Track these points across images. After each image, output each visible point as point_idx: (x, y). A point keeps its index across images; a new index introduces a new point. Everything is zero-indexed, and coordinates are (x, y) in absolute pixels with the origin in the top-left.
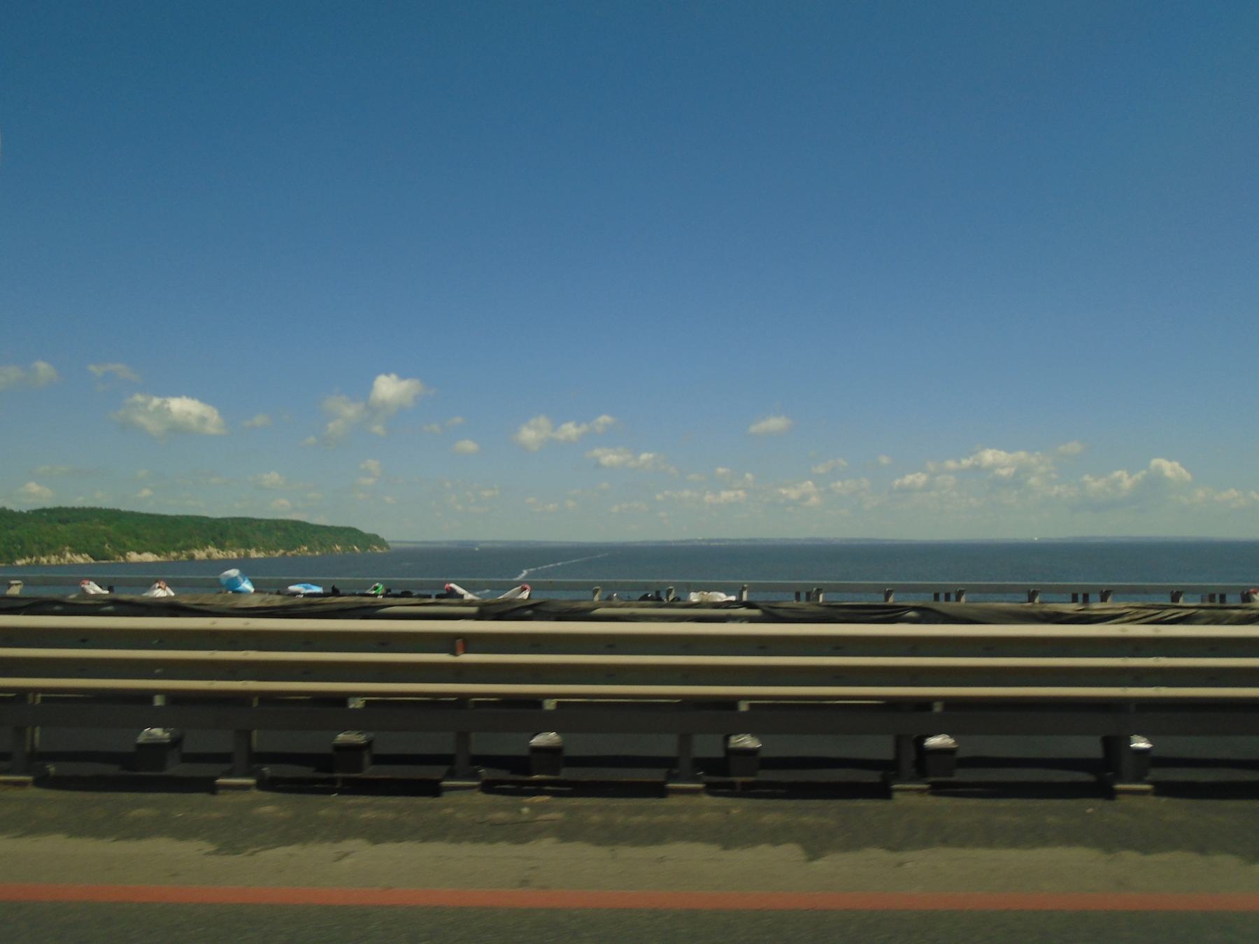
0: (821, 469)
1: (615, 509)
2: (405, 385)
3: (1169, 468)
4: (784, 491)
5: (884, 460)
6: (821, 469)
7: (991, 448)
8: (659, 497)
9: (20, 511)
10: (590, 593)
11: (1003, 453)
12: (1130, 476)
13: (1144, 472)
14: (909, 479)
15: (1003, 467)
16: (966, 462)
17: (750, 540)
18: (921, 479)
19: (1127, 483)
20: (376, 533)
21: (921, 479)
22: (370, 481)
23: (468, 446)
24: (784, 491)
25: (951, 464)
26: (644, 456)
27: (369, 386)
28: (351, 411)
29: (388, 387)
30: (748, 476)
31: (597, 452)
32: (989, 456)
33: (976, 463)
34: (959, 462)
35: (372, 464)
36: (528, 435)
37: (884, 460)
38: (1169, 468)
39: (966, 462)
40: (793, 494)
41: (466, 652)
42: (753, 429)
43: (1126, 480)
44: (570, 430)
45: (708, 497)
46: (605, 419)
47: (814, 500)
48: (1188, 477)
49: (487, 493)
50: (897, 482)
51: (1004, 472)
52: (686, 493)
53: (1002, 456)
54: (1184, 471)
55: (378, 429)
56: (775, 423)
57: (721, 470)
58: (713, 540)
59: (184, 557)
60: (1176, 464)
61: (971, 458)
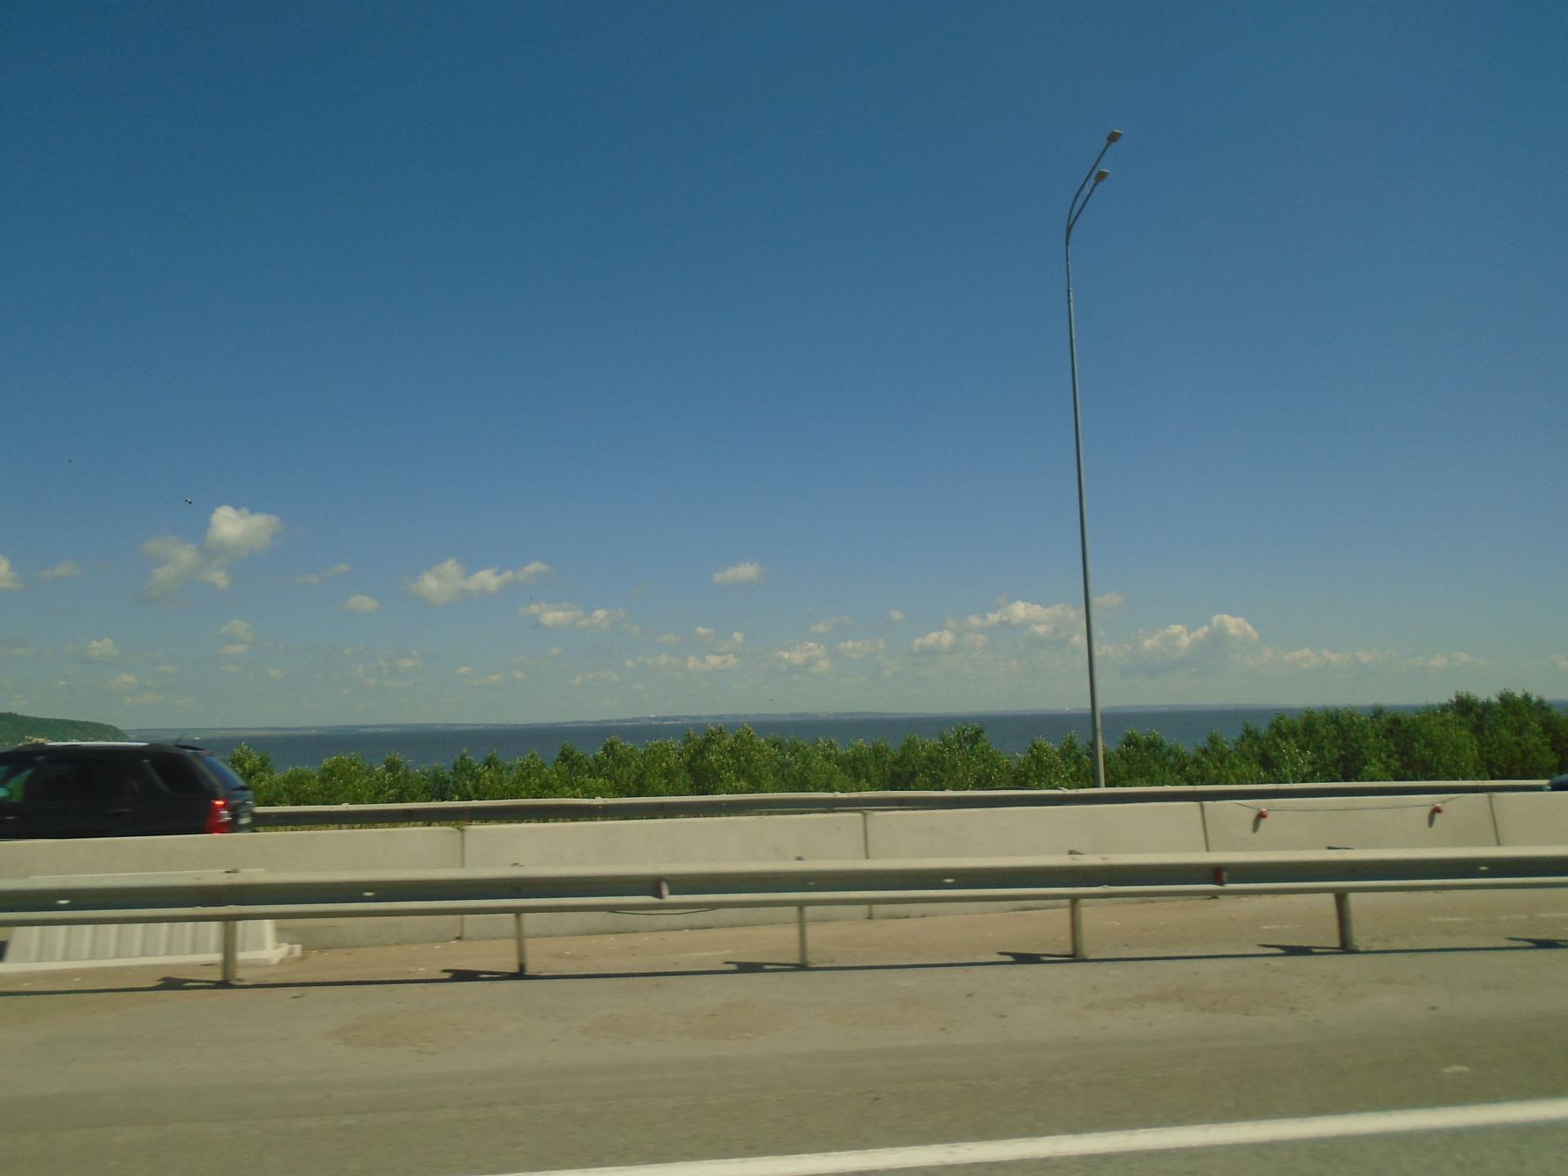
0: (821, 628)
1: (578, 680)
2: (258, 520)
3: (1233, 624)
4: (786, 655)
5: (897, 615)
6: (821, 628)
7: (1023, 601)
8: (629, 663)
9: (1376, 704)
11: (1037, 607)
12: (1189, 635)
13: (1206, 629)
14: (932, 638)
15: (1038, 624)
16: (994, 618)
17: (860, 713)
18: (947, 638)
19: (1185, 641)
21: (947, 638)
22: (240, 649)
23: (364, 602)
24: (786, 655)
25: (975, 620)
26: (600, 614)
27: (206, 524)
28: (185, 555)
29: (229, 524)
30: (738, 636)
31: (534, 609)
32: (1020, 610)
33: (1005, 619)
34: (984, 617)
35: (239, 626)
36: (430, 584)
37: (897, 615)
38: (1233, 624)
39: (994, 618)
40: (797, 657)
41: (1294, 782)
42: (718, 577)
43: (1183, 636)
44: (487, 579)
45: (692, 662)
46: (535, 567)
47: (823, 665)
48: (1255, 635)
49: (407, 663)
50: (917, 642)
51: (1041, 630)
52: (664, 659)
53: (1036, 610)
54: (1249, 627)
55: (219, 578)
56: (747, 571)
57: (701, 630)
58: (665, 719)
59: (1154, 730)
60: (1241, 620)
61: (999, 614)
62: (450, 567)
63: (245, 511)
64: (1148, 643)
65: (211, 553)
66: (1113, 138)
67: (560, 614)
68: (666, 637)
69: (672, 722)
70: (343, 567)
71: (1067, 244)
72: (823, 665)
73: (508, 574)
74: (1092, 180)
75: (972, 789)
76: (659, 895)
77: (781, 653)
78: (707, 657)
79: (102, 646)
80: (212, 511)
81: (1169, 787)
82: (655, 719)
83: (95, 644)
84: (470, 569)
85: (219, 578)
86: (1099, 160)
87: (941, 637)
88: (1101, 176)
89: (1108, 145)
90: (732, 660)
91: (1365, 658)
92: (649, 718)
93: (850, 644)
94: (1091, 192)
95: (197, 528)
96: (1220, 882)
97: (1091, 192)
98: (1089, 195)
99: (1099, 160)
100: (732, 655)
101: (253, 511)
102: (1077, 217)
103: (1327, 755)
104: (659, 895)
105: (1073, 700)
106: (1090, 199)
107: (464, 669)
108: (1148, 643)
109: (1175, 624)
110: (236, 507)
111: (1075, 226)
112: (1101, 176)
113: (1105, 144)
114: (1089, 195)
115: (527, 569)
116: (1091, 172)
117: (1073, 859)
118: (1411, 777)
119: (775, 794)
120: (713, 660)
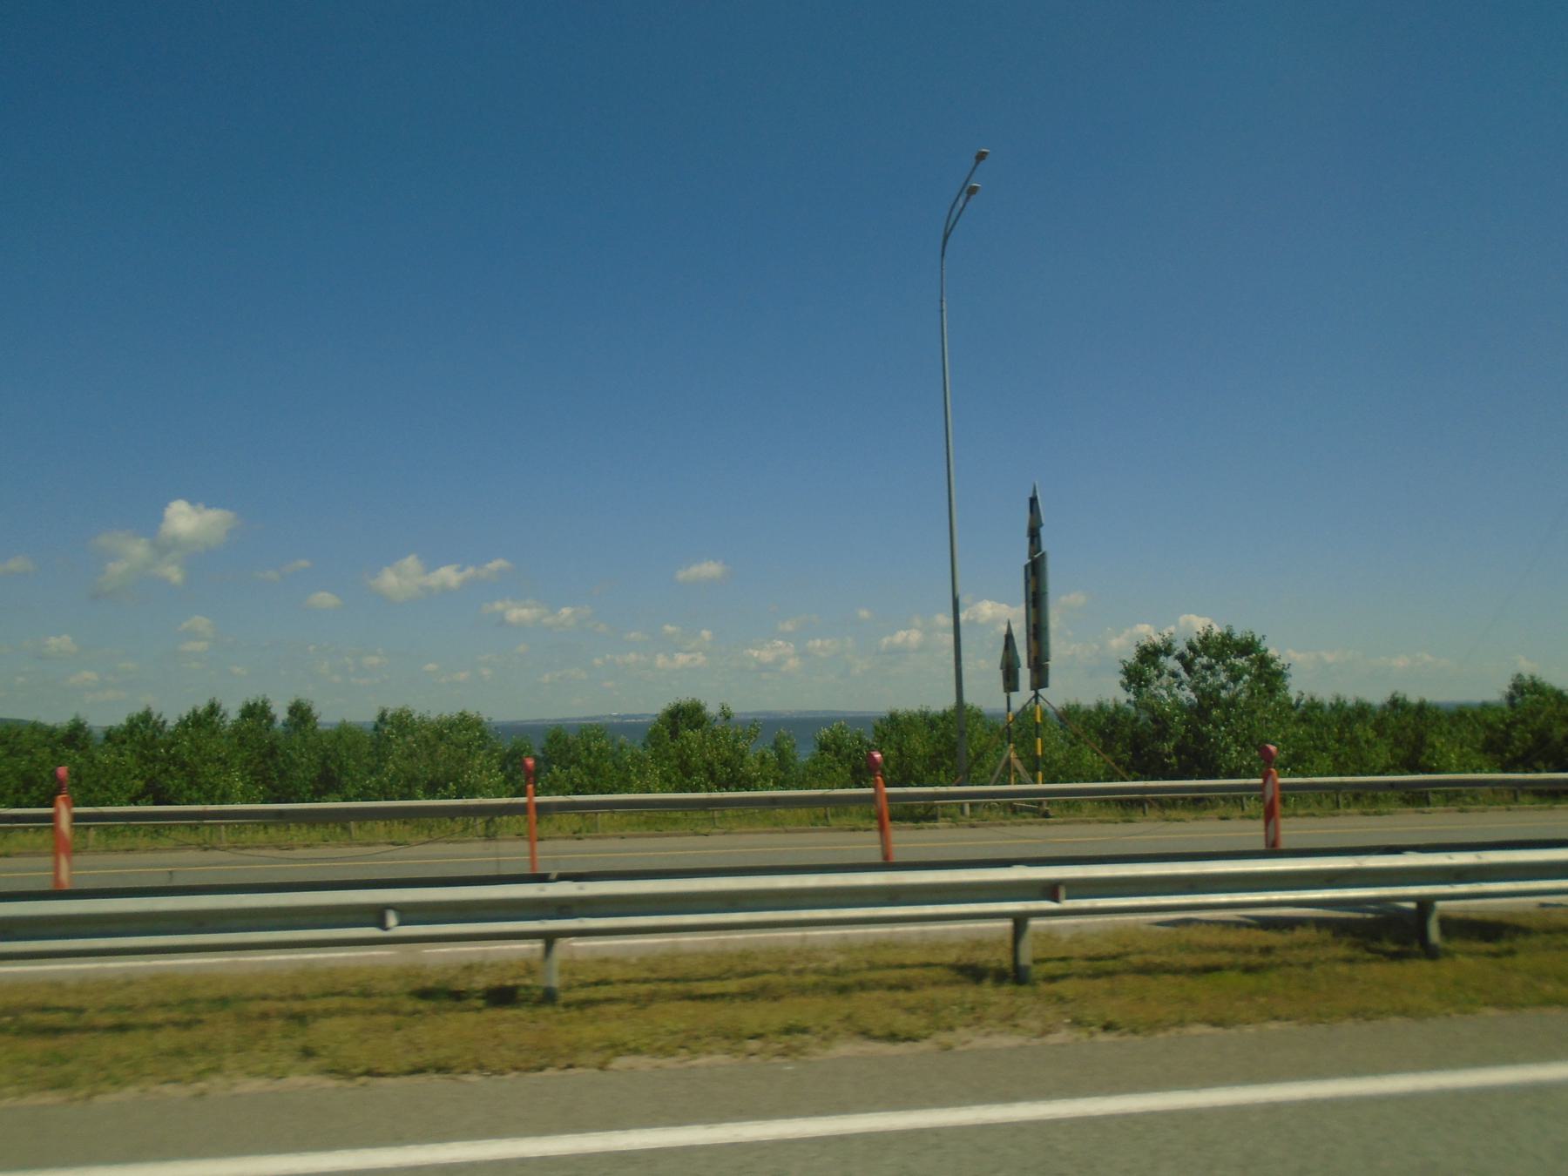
0: (788, 627)
2: (214, 516)
4: (756, 654)
5: (864, 614)
7: (989, 600)
8: (597, 661)
10: (1399, 716)
11: (1004, 606)
14: (900, 636)
17: (824, 712)
18: (915, 636)
20: (393, 706)
21: (915, 636)
22: (201, 646)
23: (325, 599)
24: (756, 654)
26: (566, 611)
27: (160, 518)
28: (139, 549)
29: (183, 519)
31: (499, 606)
33: (971, 618)
35: (200, 622)
36: (389, 580)
37: (864, 614)
40: (767, 656)
42: (681, 575)
44: (449, 575)
45: (661, 660)
47: (793, 663)
50: (885, 640)
52: (632, 657)
55: (174, 574)
56: (710, 569)
57: (669, 628)
62: (411, 562)
63: (201, 506)
64: (1115, 642)
65: (165, 548)
66: (981, 156)
67: (525, 612)
68: (633, 635)
69: (633, 720)
70: (304, 563)
71: (943, 255)
72: (793, 663)
73: (470, 571)
74: (964, 195)
75: (995, 784)
76: (382, 925)
77: (751, 651)
78: (676, 655)
79: (59, 642)
80: (167, 505)
81: (481, 799)
82: (616, 717)
83: (53, 640)
84: (431, 565)
85: (174, 574)
86: (971, 174)
87: (909, 635)
88: (973, 191)
89: (977, 163)
90: (701, 658)
91: (1329, 658)
92: (611, 716)
93: (818, 643)
94: (964, 206)
95: (149, 521)
96: (1055, 899)
97: (964, 206)
98: (962, 209)
99: (971, 174)
100: (700, 653)
101: (209, 506)
102: (953, 226)
103: (333, 767)
104: (382, 925)
105: (941, 701)
106: (963, 213)
107: (431, 667)
108: (1115, 642)
109: (1143, 623)
110: (192, 502)
111: (953, 233)
112: (973, 191)
113: (974, 164)
114: (962, 209)
115: (489, 566)
116: (964, 188)
117: (581, 888)
118: (1030, 780)
119: (442, 800)
120: (682, 659)
